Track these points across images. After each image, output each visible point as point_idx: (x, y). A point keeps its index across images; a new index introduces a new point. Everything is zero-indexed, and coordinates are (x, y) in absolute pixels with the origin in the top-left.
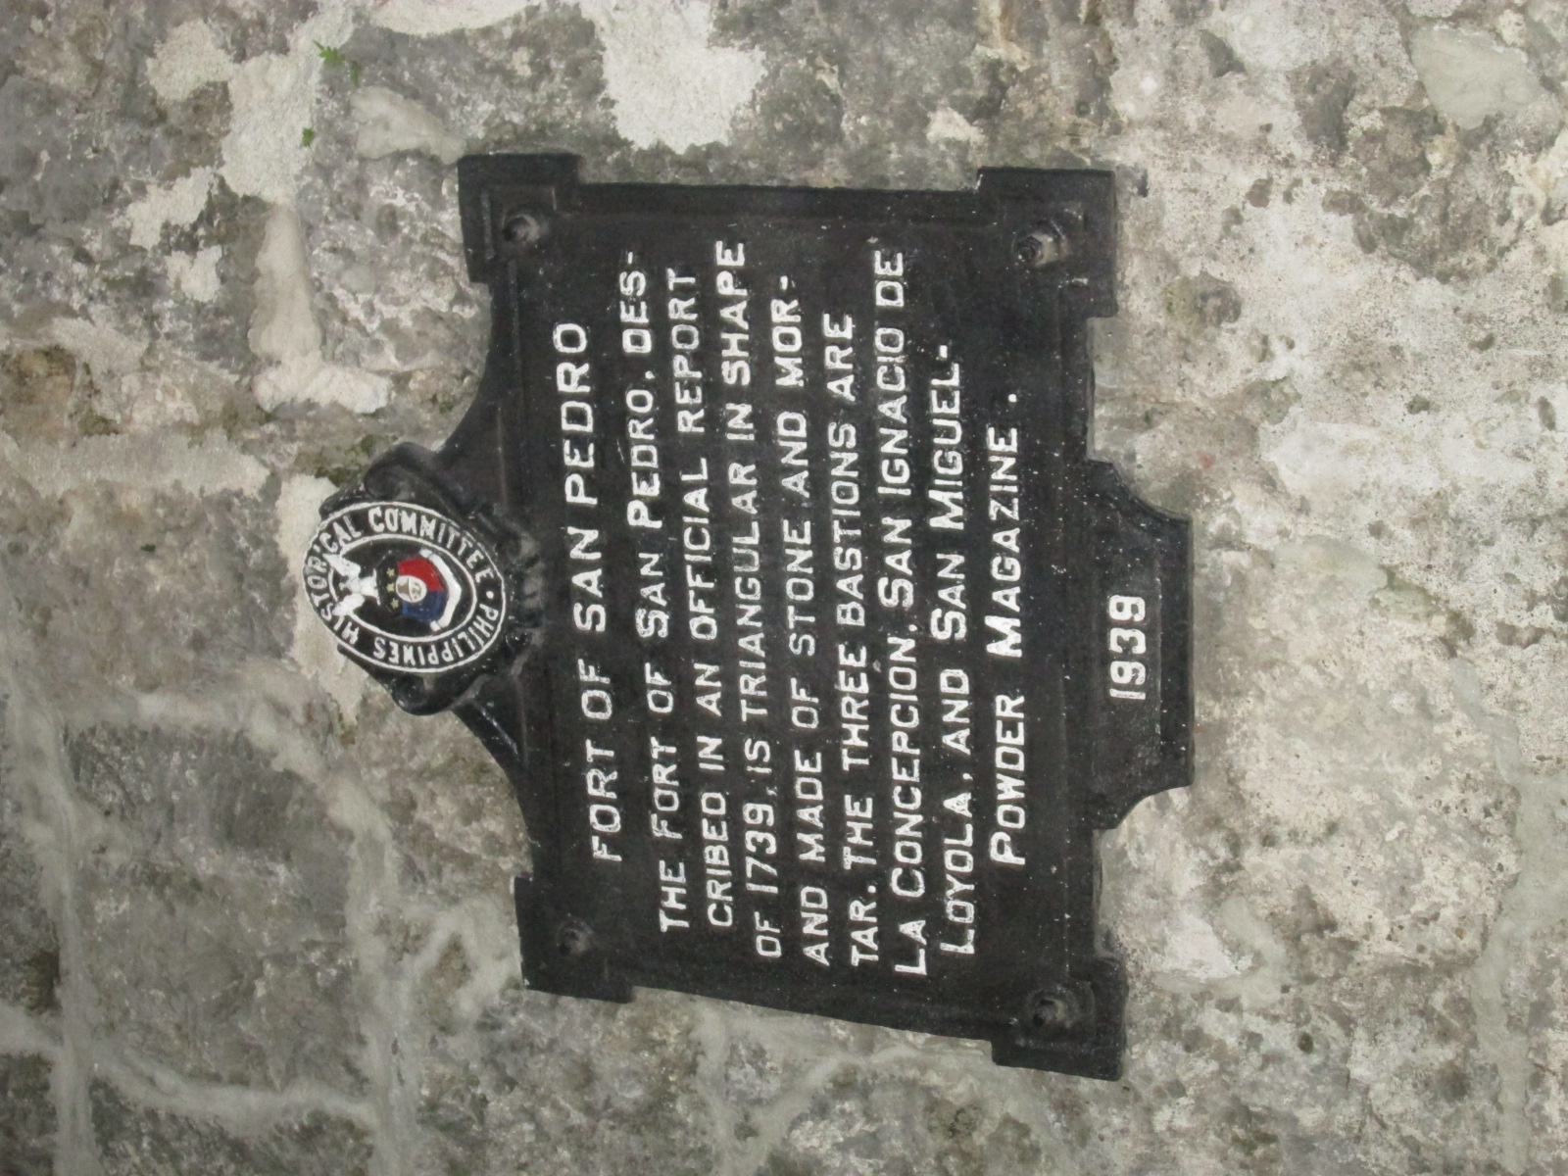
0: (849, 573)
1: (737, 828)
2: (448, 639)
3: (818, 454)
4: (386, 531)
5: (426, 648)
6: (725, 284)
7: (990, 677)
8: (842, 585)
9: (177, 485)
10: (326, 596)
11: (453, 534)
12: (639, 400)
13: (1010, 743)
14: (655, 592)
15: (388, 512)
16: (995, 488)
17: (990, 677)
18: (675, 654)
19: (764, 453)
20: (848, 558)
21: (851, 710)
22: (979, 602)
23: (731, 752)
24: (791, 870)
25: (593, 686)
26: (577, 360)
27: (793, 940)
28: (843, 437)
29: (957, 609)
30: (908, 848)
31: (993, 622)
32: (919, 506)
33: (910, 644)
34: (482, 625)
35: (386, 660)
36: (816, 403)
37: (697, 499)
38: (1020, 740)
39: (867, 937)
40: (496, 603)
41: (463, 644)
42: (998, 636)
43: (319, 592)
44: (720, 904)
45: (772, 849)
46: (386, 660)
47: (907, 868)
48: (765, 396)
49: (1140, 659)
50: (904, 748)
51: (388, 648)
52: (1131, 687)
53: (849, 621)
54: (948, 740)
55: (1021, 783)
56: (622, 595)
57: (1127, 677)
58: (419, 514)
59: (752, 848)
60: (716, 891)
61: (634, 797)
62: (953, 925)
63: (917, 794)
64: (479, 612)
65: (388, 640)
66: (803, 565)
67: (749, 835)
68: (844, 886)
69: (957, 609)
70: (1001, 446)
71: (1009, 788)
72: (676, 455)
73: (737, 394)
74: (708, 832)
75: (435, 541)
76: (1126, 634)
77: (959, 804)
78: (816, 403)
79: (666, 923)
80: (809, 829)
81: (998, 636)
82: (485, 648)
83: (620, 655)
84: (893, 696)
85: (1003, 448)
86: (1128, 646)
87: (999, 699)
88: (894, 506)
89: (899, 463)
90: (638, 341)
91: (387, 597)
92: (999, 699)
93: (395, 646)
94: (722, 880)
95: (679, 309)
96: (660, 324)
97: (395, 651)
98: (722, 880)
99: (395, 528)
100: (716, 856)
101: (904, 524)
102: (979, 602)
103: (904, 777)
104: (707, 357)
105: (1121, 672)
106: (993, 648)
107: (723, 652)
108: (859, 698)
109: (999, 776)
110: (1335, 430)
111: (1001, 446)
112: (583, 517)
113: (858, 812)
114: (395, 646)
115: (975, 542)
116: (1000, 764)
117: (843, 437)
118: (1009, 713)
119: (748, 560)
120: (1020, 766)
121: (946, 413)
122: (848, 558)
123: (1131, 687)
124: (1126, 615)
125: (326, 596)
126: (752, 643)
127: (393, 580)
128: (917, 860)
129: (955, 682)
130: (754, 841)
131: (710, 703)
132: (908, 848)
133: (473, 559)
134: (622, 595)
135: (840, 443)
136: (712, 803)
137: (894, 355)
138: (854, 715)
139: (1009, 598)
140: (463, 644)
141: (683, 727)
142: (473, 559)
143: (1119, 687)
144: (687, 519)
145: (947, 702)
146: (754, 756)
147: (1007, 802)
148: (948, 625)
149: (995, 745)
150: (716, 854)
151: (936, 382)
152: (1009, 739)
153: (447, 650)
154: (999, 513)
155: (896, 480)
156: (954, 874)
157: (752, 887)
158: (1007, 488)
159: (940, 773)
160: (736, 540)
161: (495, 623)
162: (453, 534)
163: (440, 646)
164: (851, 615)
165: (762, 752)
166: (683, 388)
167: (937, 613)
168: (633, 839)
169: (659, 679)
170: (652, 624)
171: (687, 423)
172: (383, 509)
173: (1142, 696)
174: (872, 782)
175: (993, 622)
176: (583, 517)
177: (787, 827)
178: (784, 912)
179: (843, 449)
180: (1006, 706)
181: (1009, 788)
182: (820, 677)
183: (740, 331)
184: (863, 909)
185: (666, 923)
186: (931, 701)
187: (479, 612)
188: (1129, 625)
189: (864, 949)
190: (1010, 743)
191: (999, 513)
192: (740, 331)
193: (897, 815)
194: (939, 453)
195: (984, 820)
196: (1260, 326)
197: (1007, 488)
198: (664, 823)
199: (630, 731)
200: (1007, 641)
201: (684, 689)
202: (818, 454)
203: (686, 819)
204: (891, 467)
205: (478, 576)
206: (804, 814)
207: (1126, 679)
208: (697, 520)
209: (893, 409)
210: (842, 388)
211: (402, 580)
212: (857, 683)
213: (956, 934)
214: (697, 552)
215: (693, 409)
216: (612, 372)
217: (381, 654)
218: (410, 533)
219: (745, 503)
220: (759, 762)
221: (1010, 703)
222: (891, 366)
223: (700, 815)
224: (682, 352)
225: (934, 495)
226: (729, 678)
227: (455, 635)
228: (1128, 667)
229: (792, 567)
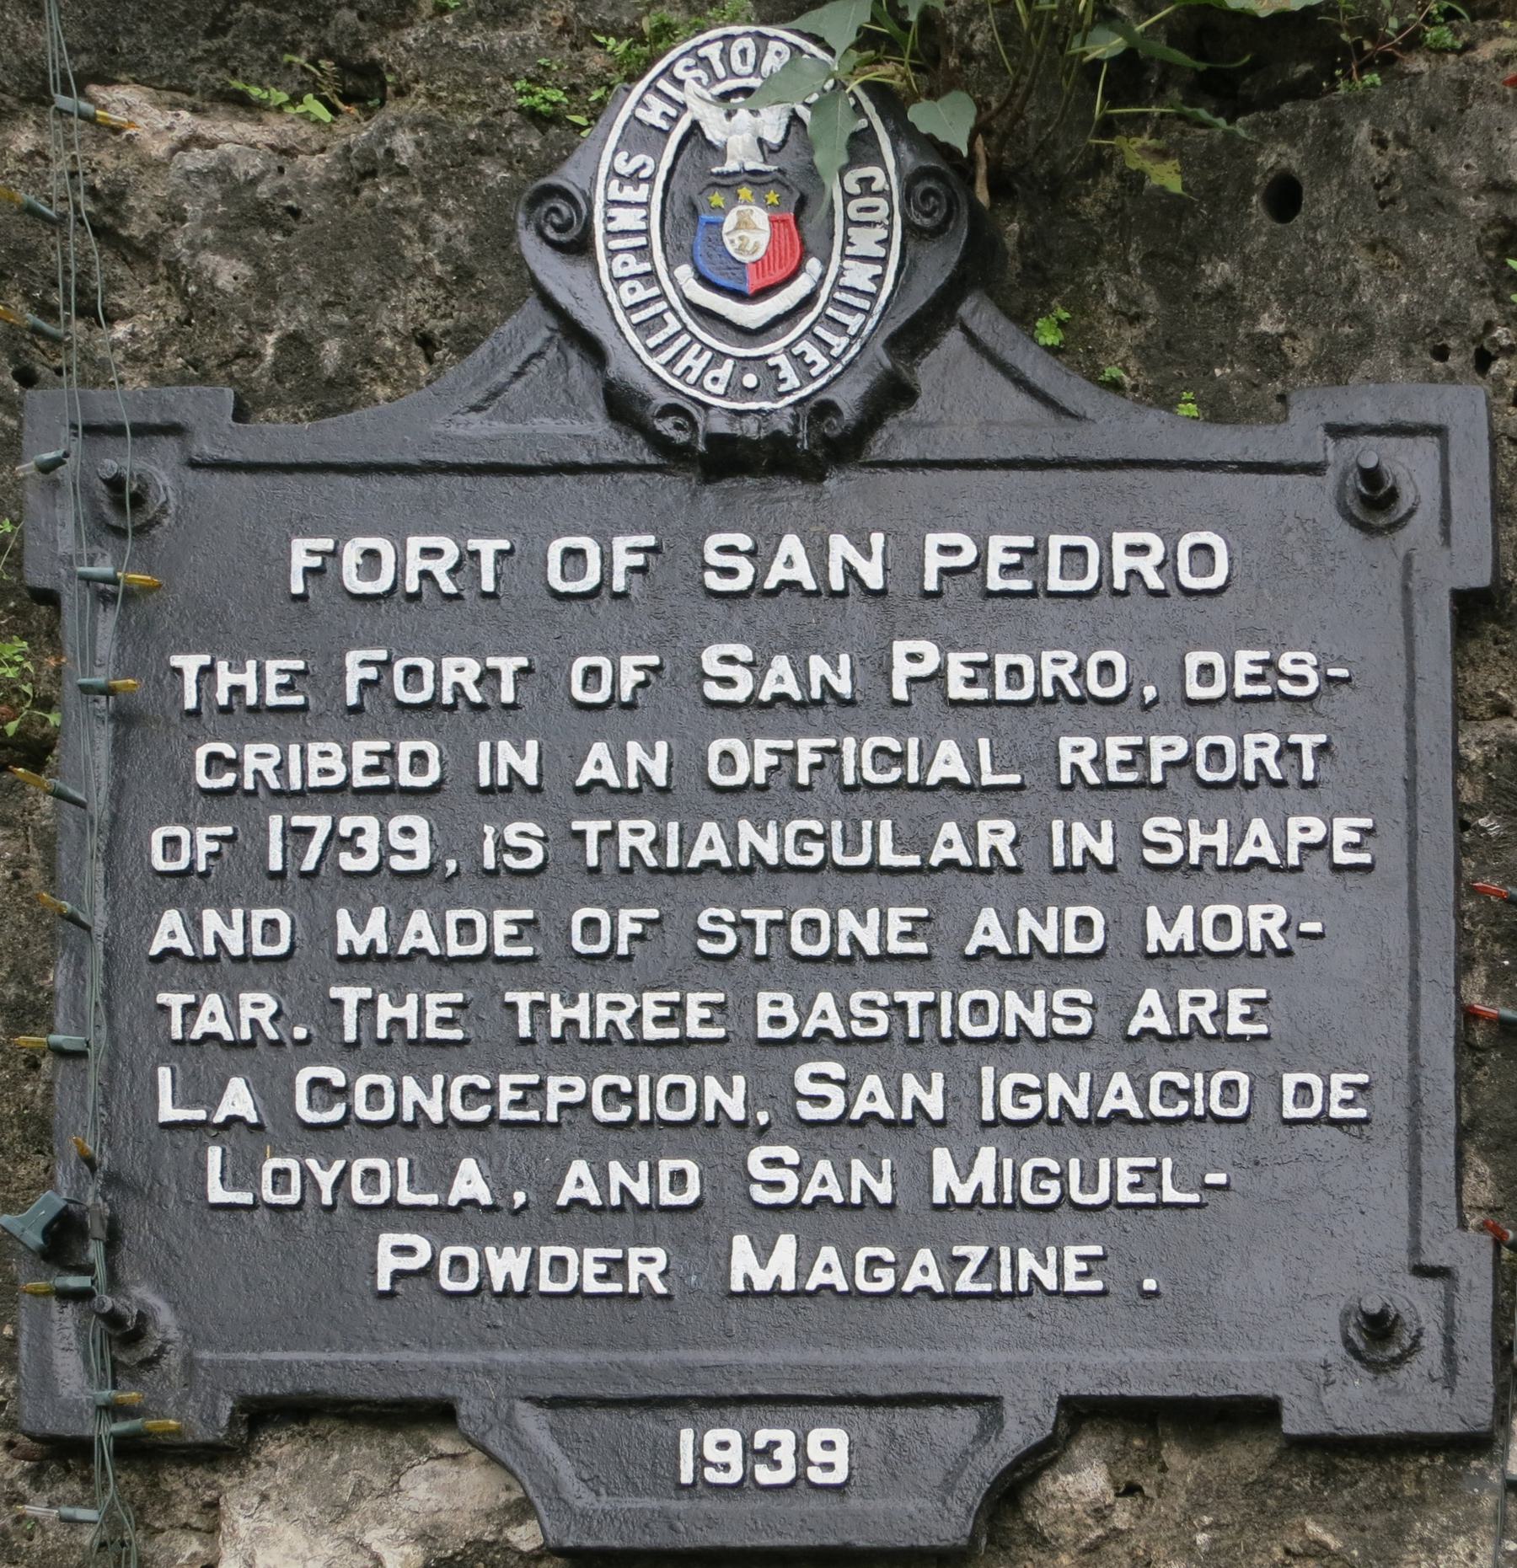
0: (846, 1015)
1: (386, 798)
2: (663, 296)
3: (1028, 967)
4: (848, 197)
5: (643, 252)
6: (1305, 828)
7: (693, 1230)
8: (825, 1000)
10: (720, 71)
11: (854, 322)
12: (1111, 669)
13: (586, 1268)
14: (781, 678)
15: (881, 202)
16: (1005, 1254)
17: (693, 1230)
18: (674, 702)
19: (1030, 879)
20: (868, 1010)
21: (596, 1011)
22: (812, 1219)
23: (509, 795)
24: (318, 888)
25: (606, 559)
26: (1167, 565)
27: (188, 888)
28: (1062, 1008)
29: (802, 1188)
30: (376, 1095)
31: (786, 1245)
32: (966, 1127)
33: (737, 1112)
34: (694, 361)
35: (613, 173)
37: (949, 762)
38: (591, 1286)
39: (212, 1018)
40: (735, 389)
41: (658, 320)
42: (764, 1252)
43: (725, 54)
44: (236, 764)
45: (348, 862)
46: (613, 173)
47: (345, 1092)
48: (1132, 881)
49: (749, 1475)
50: (555, 1096)
51: (634, 179)
52: (701, 1461)
53: (765, 1011)
54: (579, 1168)
55: (519, 1286)
58: (883, 261)
59: (346, 827)
60: (259, 759)
61: (405, 612)
62: (257, 1172)
63: (481, 1113)
64: (719, 357)
65: (650, 180)
66: (429, 1092)
67: (370, 823)
69: (802, 1188)
70: (1072, 1266)
71: (508, 1265)
73: (1131, 839)
74: (363, 751)
75: (837, 286)
76: (785, 1454)
77: (470, 1182)
78: (1122, 965)
79: (190, 664)
80: (395, 932)
81: (764, 1252)
82: (655, 364)
84: (644, 1081)
85: (1067, 1266)
86: (767, 1454)
87: (659, 1254)
88: (963, 1094)
89: (1035, 1102)
90: (1223, 668)
91: (729, 183)
92: (659, 1254)
93: (641, 194)
94: (281, 768)
95: (1260, 749)
96: (1241, 709)
97: (629, 193)
98: (281, 768)
99: (853, 215)
100: (323, 762)
101: (935, 1106)
102: (812, 1219)
103: (506, 1095)
104: (1185, 788)
105: (723, 1445)
106: (741, 1245)
107: (685, 796)
108: (636, 1019)
109: (526, 1251)
111: (1072, 1266)
112: (904, 558)
113: (428, 1011)
114: (641, 194)
116: (547, 1253)
117: (1062, 1008)
118: (635, 1268)
119: (852, 844)
120: (546, 1285)
121: (1119, 1176)
122: (868, 1010)
123: (701, 1461)
124: (815, 1453)
125: (720, 71)
126: (710, 844)
127: (762, 203)
128: (361, 1111)
129: (677, 1178)
130: (359, 831)
131: (598, 764)
132: (376, 1095)
133: (813, 354)
135: (1059, 1007)
136: (420, 759)
137: (1206, 1099)
138: (604, 1015)
139: (828, 1270)
140: (658, 320)
142: (813, 354)
143: (698, 1446)
144: (913, 744)
145: (643, 1167)
146: (513, 841)
147: (482, 1259)
149: (580, 1245)
150: (326, 763)
151: (1167, 1164)
152: (592, 1268)
153: (642, 294)
154: (964, 1260)
155: (1000, 1091)
156: (346, 1171)
157: (276, 823)
158: (1006, 1271)
160: (886, 826)
161: (698, 384)
162: (854, 322)
163: (650, 277)
164: (772, 1008)
165: (524, 852)
166: (1134, 749)
167: (791, 1155)
169: (630, 678)
171: (1075, 752)
172: (886, 194)
173: (686, 1477)
174: (484, 1041)
175: (786, 1245)
176: (904, 558)
177: (398, 887)
178: (233, 879)
179: (1051, 1014)
180: (648, 1266)
181: (508, 1265)
182: (663, 959)
183: (1232, 851)
184: (264, 1016)
185: (190, 664)
186: (641, 1137)
187: (719, 357)
188: (802, 1458)
189: (191, 1010)
190: (586, 1268)
191: (964, 1260)
192: (1232, 851)
193: (438, 1081)
194: (1055, 1168)
195: (450, 1219)
197: (1006, 1271)
198: (371, 673)
201: (618, 716)
202: (1028, 967)
203: (376, 711)
204: (1027, 1090)
205: (781, 360)
206: (419, 919)
207: (711, 1453)
208: (913, 760)
209: (1120, 1095)
210: (1150, 1012)
211: (760, 217)
212: (659, 1021)
213: (240, 1173)
214: (858, 757)
215: (1099, 761)
217: (624, 169)
218: (847, 241)
219: (949, 844)
220: (502, 847)
221: (653, 1272)
222: (1188, 1094)
223: (394, 737)
224: (1192, 750)
225: (987, 1156)
226: (641, 796)
227: (672, 309)
228: (734, 1456)
229: (847, 919)
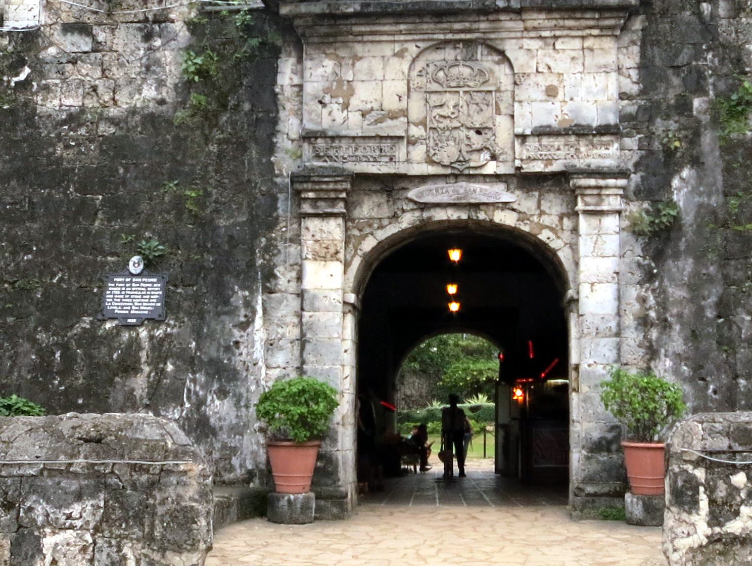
9: (143, 548)
18: (131, 287)
36: (150, 299)
56: (136, 283)
57: (134, 321)
61: (120, 282)
68: (113, 298)
72: (146, 288)
78: (150, 299)
83: (131, 282)
110: (289, 214)
115: (139, 310)
134: (136, 283)
141: (126, 287)
148: (134, 308)
159: (122, 306)
168: (116, 282)
170: (134, 285)
196: (490, 134)
199: (125, 282)
200: (132, 312)
216: (153, 283)
